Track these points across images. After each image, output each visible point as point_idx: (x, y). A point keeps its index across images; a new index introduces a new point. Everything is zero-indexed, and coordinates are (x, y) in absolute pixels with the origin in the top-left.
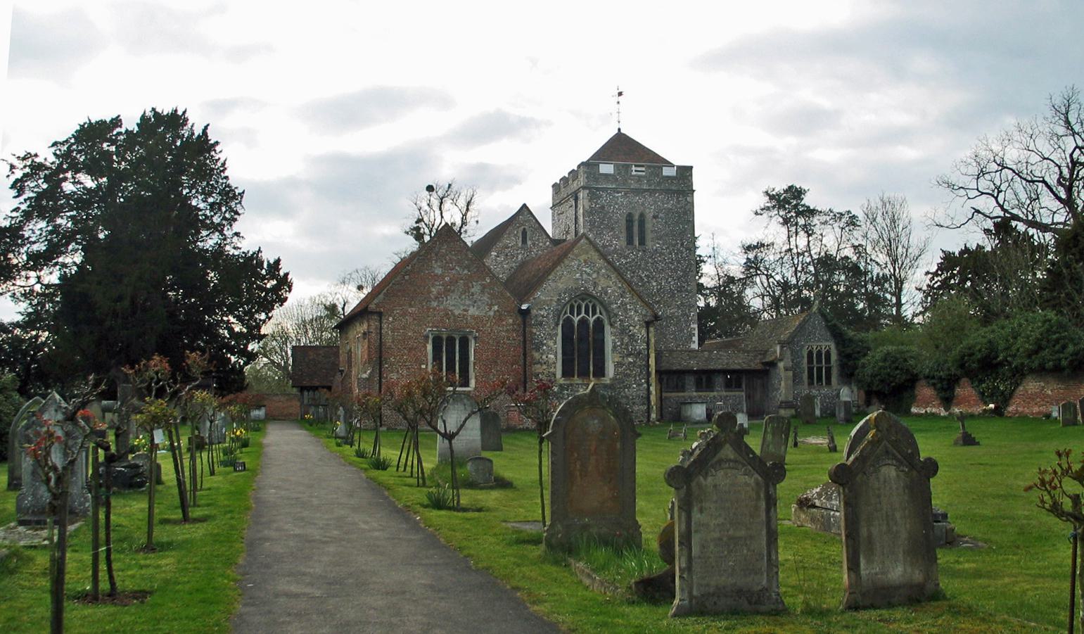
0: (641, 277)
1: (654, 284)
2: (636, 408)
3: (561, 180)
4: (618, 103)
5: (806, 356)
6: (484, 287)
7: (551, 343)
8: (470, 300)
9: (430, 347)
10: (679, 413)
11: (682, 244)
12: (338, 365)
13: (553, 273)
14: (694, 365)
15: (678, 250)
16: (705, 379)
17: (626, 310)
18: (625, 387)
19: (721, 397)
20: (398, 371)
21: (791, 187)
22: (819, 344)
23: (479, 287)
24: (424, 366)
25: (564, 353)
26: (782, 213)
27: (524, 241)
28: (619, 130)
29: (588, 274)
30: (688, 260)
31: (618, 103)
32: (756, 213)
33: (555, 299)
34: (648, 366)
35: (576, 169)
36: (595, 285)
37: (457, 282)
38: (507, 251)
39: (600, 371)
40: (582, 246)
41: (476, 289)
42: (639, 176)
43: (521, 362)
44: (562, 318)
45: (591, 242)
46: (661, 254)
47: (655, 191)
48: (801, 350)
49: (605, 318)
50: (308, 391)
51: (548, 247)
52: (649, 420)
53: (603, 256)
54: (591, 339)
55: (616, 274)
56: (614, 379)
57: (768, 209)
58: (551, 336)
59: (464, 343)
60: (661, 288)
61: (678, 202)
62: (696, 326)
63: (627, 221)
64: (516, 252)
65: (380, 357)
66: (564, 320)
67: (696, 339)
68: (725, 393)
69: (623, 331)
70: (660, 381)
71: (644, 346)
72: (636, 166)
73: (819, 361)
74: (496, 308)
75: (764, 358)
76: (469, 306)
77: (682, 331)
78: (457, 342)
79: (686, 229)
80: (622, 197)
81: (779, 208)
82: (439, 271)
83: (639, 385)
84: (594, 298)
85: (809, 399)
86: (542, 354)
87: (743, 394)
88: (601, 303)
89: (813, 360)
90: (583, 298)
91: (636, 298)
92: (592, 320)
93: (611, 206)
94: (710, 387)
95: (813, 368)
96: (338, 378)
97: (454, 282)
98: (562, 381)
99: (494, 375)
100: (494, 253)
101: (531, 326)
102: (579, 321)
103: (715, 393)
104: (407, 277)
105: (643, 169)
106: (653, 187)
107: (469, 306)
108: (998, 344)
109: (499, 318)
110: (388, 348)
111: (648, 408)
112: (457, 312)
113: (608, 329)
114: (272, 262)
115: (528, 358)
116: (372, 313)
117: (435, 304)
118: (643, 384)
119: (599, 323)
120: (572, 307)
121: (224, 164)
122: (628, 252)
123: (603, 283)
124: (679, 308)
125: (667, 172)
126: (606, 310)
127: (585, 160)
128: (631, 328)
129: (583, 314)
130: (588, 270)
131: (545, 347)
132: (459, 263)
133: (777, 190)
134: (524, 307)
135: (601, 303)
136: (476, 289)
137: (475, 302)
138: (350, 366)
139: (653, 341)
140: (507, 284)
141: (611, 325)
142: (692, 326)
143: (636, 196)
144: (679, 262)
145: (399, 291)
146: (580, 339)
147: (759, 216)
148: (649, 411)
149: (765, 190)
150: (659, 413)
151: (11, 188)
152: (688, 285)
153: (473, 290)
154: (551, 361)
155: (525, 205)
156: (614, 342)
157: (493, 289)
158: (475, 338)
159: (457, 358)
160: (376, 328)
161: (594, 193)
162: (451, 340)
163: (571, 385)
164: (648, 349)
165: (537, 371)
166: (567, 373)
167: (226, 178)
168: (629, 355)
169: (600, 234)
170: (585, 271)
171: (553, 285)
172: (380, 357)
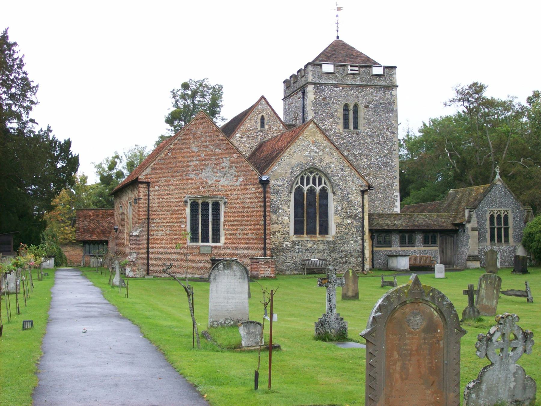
0: (355, 155)
1: (365, 160)
3: (291, 77)
4: (337, 15)
5: (488, 219)
6: (232, 162)
7: (285, 207)
9: (188, 210)
10: (387, 264)
11: (388, 129)
12: (113, 224)
13: (287, 151)
14: (400, 224)
15: (385, 133)
16: (407, 236)
17: (346, 182)
18: (344, 243)
19: (419, 249)
21: (475, 84)
22: (499, 209)
23: (228, 162)
24: (183, 226)
25: (296, 215)
26: (466, 104)
27: (262, 125)
28: (338, 37)
29: (316, 152)
31: (337, 15)
33: (289, 172)
34: (363, 226)
35: (303, 68)
36: (321, 161)
37: (210, 158)
38: (249, 133)
39: (324, 230)
40: (311, 129)
41: (226, 163)
42: (353, 74)
43: (262, 224)
44: (295, 187)
45: (318, 126)
47: (366, 86)
48: (485, 213)
49: (328, 187)
50: (89, 245)
51: (281, 130)
52: (363, 270)
53: (327, 137)
54: (317, 204)
55: (337, 152)
56: (336, 236)
57: (454, 101)
58: (286, 202)
59: (216, 206)
60: (371, 164)
61: (385, 95)
62: (398, 194)
63: (344, 110)
64: (255, 134)
65: (148, 219)
66: (296, 189)
67: (398, 204)
68: (423, 249)
69: (344, 198)
70: (372, 238)
72: (351, 66)
73: (499, 223)
75: (454, 220)
76: (220, 177)
77: (387, 197)
78: (210, 206)
79: (390, 117)
80: (340, 91)
81: (464, 101)
82: (195, 149)
83: (355, 242)
84: (320, 171)
85: (493, 253)
86: (278, 216)
87: (437, 248)
88: (326, 175)
89: (501, 221)
90: (312, 172)
91: (353, 171)
92: (318, 189)
93: (331, 98)
94: (411, 243)
95: (494, 228)
96: (113, 235)
97: (208, 158)
99: (240, 233)
100: (238, 135)
101: (270, 193)
102: (308, 190)
103: (415, 248)
104: (170, 154)
105: (357, 69)
106: (364, 83)
111: (363, 260)
112: (210, 182)
113: (331, 196)
114: (63, 142)
115: (268, 220)
116: (142, 183)
117: (192, 176)
119: (324, 192)
120: (302, 178)
121: (21, 61)
123: (327, 159)
125: (377, 71)
126: (330, 181)
127: (310, 61)
128: (350, 196)
129: (311, 184)
130: (316, 149)
131: (280, 211)
132: (212, 142)
133: (462, 86)
134: (264, 178)
135: (326, 175)
136: (226, 163)
137: (225, 174)
138: (123, 226)
139: (366, 206)
140: (251, 158)
141: (334, 193)
142: (395, 194)
143: (352, 90)
144: (385, 143)
145: (163, 165)
146: (309, 205)
147: (448, 107)
148: (363, 262)
149: (97, 163)
150: (371, 263)
151: (69, 139)
154: (285, 222)
155: (263, 97)
156: (336, 208)
158: (225, 203)
159: (210, 220)
162: (205, 205)
164: (363, 212)
166: (298, 231)
167: (25, 73)
168: (348, 217)
171: (287, 160)
172: (148, 219)
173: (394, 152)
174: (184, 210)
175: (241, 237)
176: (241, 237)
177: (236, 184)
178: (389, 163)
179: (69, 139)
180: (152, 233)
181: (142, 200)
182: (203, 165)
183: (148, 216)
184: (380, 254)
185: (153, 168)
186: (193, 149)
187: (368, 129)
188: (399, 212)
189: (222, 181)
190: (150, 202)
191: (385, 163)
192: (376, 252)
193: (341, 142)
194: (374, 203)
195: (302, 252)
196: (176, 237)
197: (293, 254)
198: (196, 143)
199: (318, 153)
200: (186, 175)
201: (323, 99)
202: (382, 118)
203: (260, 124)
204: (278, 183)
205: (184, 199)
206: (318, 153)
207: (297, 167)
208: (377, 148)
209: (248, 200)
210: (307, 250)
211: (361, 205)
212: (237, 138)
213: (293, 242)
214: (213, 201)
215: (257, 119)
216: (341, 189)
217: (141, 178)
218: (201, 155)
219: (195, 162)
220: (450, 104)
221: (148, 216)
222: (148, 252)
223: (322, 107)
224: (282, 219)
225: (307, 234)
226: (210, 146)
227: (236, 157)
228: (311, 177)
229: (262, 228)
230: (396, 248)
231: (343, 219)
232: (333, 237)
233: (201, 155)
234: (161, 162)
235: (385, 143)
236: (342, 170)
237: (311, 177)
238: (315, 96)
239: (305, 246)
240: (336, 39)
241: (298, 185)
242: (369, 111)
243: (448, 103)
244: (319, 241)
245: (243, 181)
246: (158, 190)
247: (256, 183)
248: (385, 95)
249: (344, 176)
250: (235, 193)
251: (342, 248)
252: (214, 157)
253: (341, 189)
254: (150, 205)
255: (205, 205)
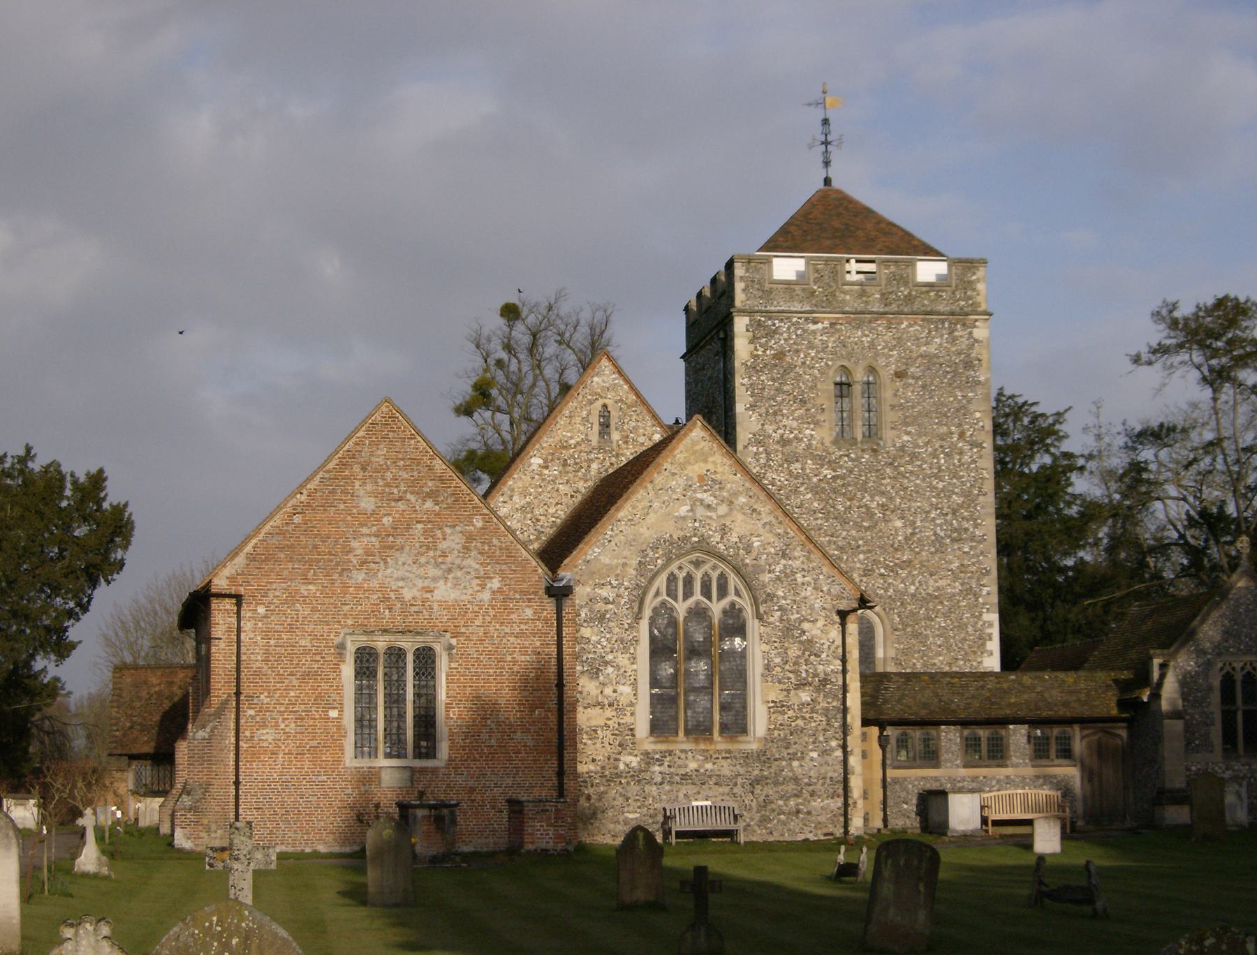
0: (868, 508)
1: (899, 524)
2: (817, 804)
6: (470, 538)
7: (623, 660)
8: (437, 565)
9: (348, 670)
15: (953, 446)
17: (794, 587)
18: (793, 757)
20: (277, 725)
24: (333, 714)
27: (605, 426)
28: (827, 181)
30: (977, 469)
32: (1137, 360)
34: (845, 711)
36: (724, 530)
37: (408, 528)
38: (566, 454)
39: (737, 725)
40: (694, 443)
41: (452, 541)
43: (553, 705)
46: (914, 456)
49: (745, 603)
58: (626, 645)
59: (426, 659)
60: (913, 534)
61: (954, 340)
62: (994, 617)
67: (994, 645)
69: (788, 631)
71: (838, 665)
74: (495, 584)
76: (435, 579)
83: (825, 753)
84: (721, 558)
88: (738, 571)
91: (816, 556)
92: (716, 608)
93: (797, 351)
95: (1235, 713)
97: (402, 527)
98: (649, 746)
100: (536, 461)
103: (1008, 771)
104: (297, 519)
106: (894, 307)
107: (435, 579)
108: (925, 705)
109: (503, 601)
110: (255, 674)
111: (846, 805)
112: (408, 594)
114: (82, 478)
117: (359, 577)
118: (832, 750)
120: (672, 579)
122: (838, 453)
124: (956, 578)
126: (749, 587)
128: (806, 626)
130: (707, 498)
131: (610, 670)
136: (452, 541)
137: (450, 570)
147: (1145, 368)
151: (101, 471)
152: (976, 526)
153: (444, 545)
154: (623, 701)
157: (490, 543)
160: (229, 631)
161: (759, 324)
163: (671, 753)
164: (844, 671)
165: (594, 723)
166: (659, 727)
168: (801, 685)
169: (775, 413)
170: (702, 501)
171: (629, 531)
173: (981, 498)
174: (336, 669)
175: (493, 742)
176: (493, 742)
177: (480, 596)
178: (966, 530)
179: (101, 471)
180: (248, 734)
181: (222, 645)
182: (391, 548)
183: (238, 686)
184: (905, 789)
185: (251, 558)
186: (363, 505)
187: (906, 438)
188: (997, 668)
189: (443, 587)
190: (243, 649)
191: (956, 530)
192: (896, 781)
193: (828, 473)
194: (924, 643)
195: (670, 783)
196: (314, 743)
197: (647, 788)
198: (369, 487)
199: (715, 510)
200: (341, 574)
201: (774, 356)
202: (943, 404)
203: (596, 428)
204: (604, 592)
205: (337, 641)
206: (715, 510)
207: (655, 549)
208: (933, 488)
209: (512, 639)
210: (685, 777)
211: (840, 650)
212: (534, 467)
213: (646, 754)
214: (359, 645)
215: (589, 413)
216: (781, 609)
217: (220, 583)
218: (385, 520)
219: (365, 540)
220: (1153, 358)
221: (238, 686)
222: (237, 783)
223: (774, 380)
224: (615, 691)
225: (688, 732)
226: (409, 496)
227: (479, 524)
228: (698, 576)
229: (553, 718)
230: (951, 770)
231: (788, 691)
232: (760, 740)
233: (385, 520)
234: (275, 541)
235: (955, 475)
236: (784, 556)
237: (698, 576)
238: (752, 346)
239: (680, 767)
240: (821, 185)
241: (659, 599)
242: (906, 386)
243: (1145, 357)
244: (719, 752)
245: (500, 590)
246: (266, 617)
247: (535, 593)
248: (954, 340)
249: (788, 575)
250: (477, 623)
251: (786, 773)
252: (420, 526)
253: (781, 609)
254: (243, 657)
255: (396, 655)
